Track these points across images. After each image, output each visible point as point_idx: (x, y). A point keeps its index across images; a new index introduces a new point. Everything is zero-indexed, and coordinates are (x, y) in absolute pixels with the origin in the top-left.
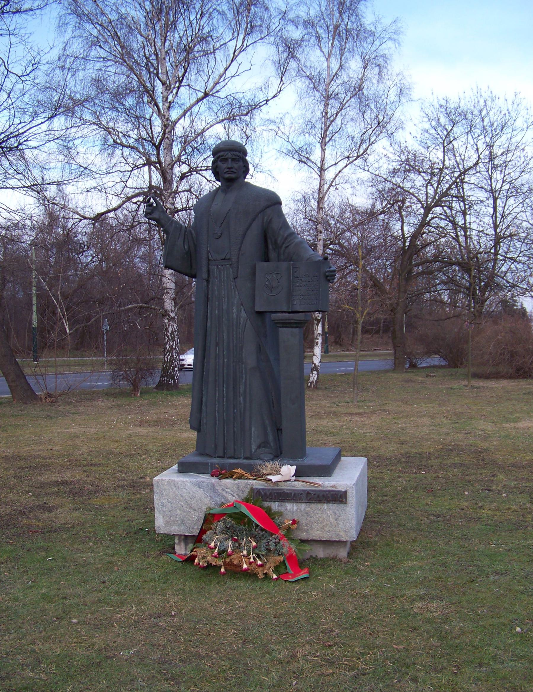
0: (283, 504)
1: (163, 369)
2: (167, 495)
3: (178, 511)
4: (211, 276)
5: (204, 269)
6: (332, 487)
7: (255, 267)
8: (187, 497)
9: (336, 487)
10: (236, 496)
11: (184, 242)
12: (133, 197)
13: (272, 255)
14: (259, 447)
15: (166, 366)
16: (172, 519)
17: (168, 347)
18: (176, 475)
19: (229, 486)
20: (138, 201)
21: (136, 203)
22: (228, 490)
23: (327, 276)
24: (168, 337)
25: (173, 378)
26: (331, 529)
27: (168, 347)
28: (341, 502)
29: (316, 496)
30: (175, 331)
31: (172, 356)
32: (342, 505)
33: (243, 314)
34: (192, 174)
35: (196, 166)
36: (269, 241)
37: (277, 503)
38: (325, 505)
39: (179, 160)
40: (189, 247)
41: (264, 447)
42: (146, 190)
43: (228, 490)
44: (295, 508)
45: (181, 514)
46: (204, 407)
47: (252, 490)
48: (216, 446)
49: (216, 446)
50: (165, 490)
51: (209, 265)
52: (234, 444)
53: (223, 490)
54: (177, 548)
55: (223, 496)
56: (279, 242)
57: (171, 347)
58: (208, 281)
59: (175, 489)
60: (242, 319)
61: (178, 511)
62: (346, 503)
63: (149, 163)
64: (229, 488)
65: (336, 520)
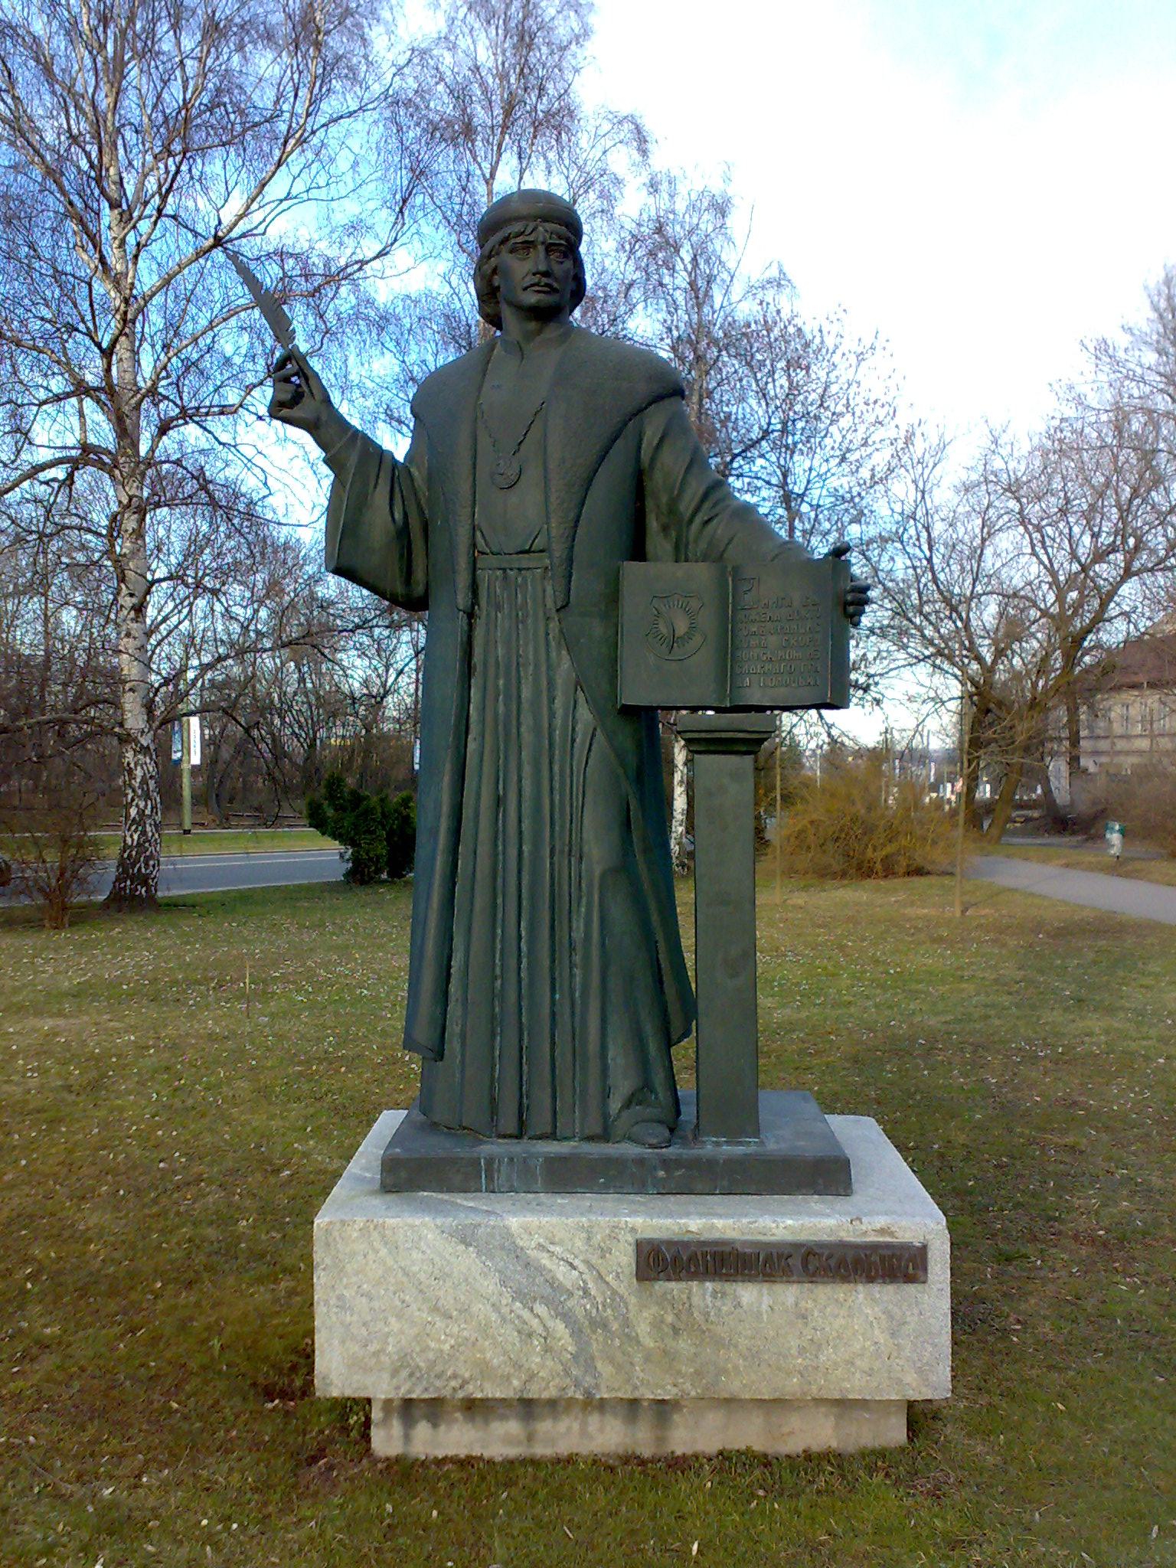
0: (729, 1287)
1: (122, 863)
2: (357, 1273)
3: (393, 1320)
4: (483, 601)
5: (463, 580)
6: (882, 1231)
7: (617, 578)
8: (422, 1277)
9: (892, 1234)
10: (582, 1267)
11: (391, 499)
12: (43, 467)
13: (657, 542)
14: (627, 1104)
15: (130, 856)
16: (372, 1348)
17: (133, 812)
18: (377, 1201)
19: (560, 1235)
20: (55, 480)
21: (47, 483)
22: (558, 1249)
23: (846, 604)
24: (134, 791)
25: (145, 883)
26: (877, 1365)
27: (133, 812)
28: (910, 1279)
29: (833, 1262)
30: (151, 777)
31: (144, 833)
32: (911, 1288)
33: (584, 714)
34: (186, 423)
35: (194, 404)
36: (650, 504)
37: (708, 1284)
38: (860, 1287)
39: (153, 391)
40: (406, 515)
41: (639, 1103)
42: (74, 453)
43: (558, 1249)
44: (766, 1301)
45: (401, 1332)
46: (453, 988)
47: (639, 1245)
48: (493, 1102)
49: (493, 1102)
50: (353, 1254)
51: (474, 570)
52: (554, 1098)
53: (541, 1247)
54: (377, 1436)
55: (541, 1269)
56: (682, 507)
57: (141, 813)
58: (471, 615)
59: (383, 1252)
60: (579, 727)
61: (393, 1320)
62: (924, 1282)
63: (81, 389)
64: (561, 1243)
65: (893, 1335)
